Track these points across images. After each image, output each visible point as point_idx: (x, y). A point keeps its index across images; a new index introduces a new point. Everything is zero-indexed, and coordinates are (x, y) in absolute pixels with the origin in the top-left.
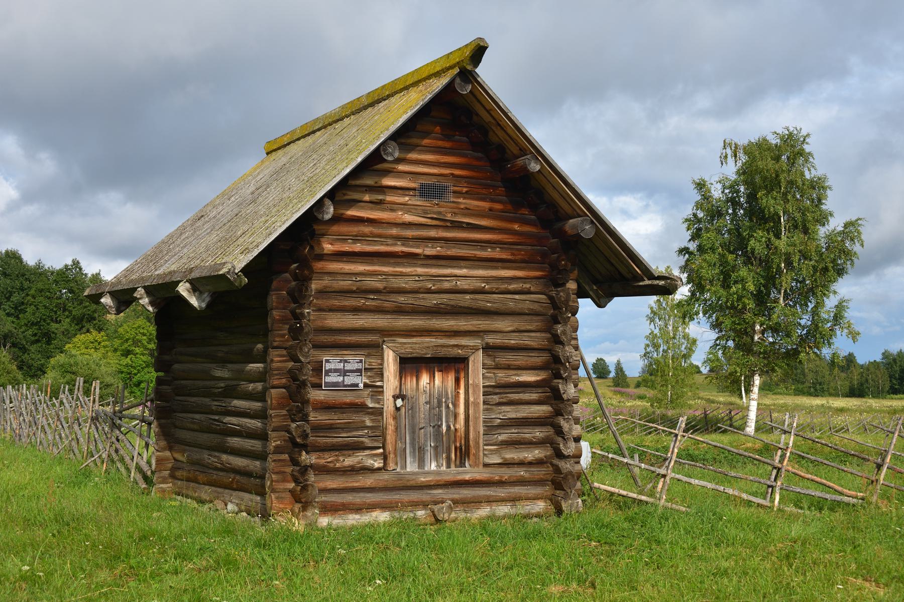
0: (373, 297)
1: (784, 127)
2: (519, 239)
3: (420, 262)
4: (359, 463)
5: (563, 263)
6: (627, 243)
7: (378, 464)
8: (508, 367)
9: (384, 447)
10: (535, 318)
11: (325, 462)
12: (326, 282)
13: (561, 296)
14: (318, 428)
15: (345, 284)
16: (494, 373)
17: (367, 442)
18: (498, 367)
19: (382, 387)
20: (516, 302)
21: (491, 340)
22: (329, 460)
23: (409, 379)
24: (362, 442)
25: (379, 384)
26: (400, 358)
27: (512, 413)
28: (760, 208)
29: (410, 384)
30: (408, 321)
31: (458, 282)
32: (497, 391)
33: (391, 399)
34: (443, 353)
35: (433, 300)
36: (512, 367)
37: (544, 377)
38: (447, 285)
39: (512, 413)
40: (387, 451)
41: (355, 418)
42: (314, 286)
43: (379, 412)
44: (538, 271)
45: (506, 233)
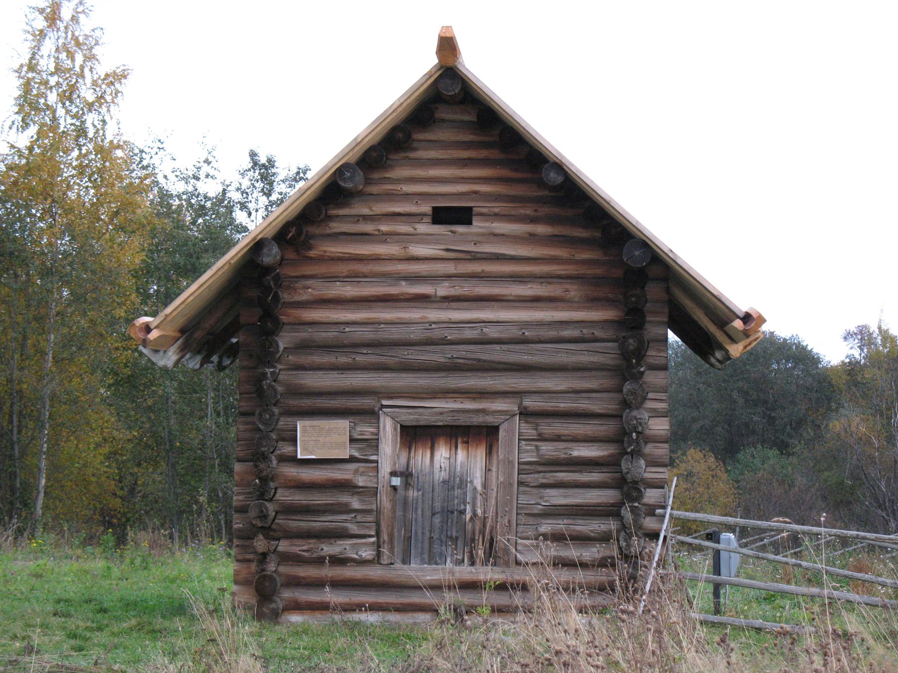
0: (365, 352)
1: (884, 327)
2: (577, 270)
3: (435, 305)
4: (341, 553)
5: (633, 299)
6: (328, 183)
7: (367, 554)
8: (558, 438)
9: (378, 535)
10: (599, 374)
11: (300, 551)
12: (305, 334)
13: (629, 344)
14: (290, 510)
15: (329, 335)
16: (536, 446)
17: (354, 529)
18: (542, 438)
19: (377, 462)
20: (567, 353)
21: (530, 403)
22: (304, 548)
23: (420, 452)
24: (346, 529)
25: (374, 458)
26: (401, 426)
27: (557, 498)
28: (868, 331)
29: (421, 459)
30: (411, 380)
31: (484, 329)
32: (541, 468)
33: (387, 476)
34: (463, 420)
35: (437, 356)
36: (563, 438)
37: (612, 451)
38: (469, 334)
39: (557, 498)
40: (381, 540)
41: (344, 498)
42: (283, 341)
43: (374, 492)
44: (578, 309)
45: (558, 264)
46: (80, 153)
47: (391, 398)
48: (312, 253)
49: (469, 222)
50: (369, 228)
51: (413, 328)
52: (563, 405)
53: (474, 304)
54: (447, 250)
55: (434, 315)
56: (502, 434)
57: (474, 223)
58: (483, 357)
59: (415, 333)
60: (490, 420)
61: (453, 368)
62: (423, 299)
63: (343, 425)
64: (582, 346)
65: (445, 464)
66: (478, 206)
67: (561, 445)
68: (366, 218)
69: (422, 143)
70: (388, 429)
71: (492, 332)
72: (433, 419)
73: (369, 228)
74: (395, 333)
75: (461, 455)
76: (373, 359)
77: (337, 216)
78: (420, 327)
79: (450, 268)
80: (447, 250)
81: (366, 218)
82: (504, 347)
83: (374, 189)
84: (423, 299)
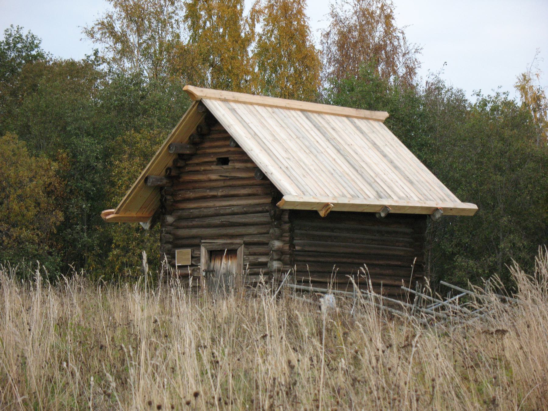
35: (217, 221)
38: (228, 211)
46: (385, 50)
47: (205, 239)
48: (181, 180)
49: (227, 164)
50: (197, 168)
51: (211, 209)
52: (256, 240)
53: (230, 198)
54: (220, 176)
55: (218, 204)
56: (238, 252)
57: (229, 164)
58: (231, 220)
59: (211, 211)
60: (233, 247)
61: (222, 225)
62: (214, 197)
63: (189, 250)
64: (259, 215)
65: (225, 266)
66: (231, 157)
67: (256, 257)
68: (198, 164)
69: (293, 112)
70: (203, 253)
71: (235, 209)
72: (217, 247)
73: (197, 168)
74: (206, 212)
75: (230, 262)
76: (199, 223)
77: (190, 164)
78: (213, 209)
79: (221, 184)
80: (220, 176)
81: (198, 164)
82: (238, 216)
83: (199, 152)
84: (214, 197)
